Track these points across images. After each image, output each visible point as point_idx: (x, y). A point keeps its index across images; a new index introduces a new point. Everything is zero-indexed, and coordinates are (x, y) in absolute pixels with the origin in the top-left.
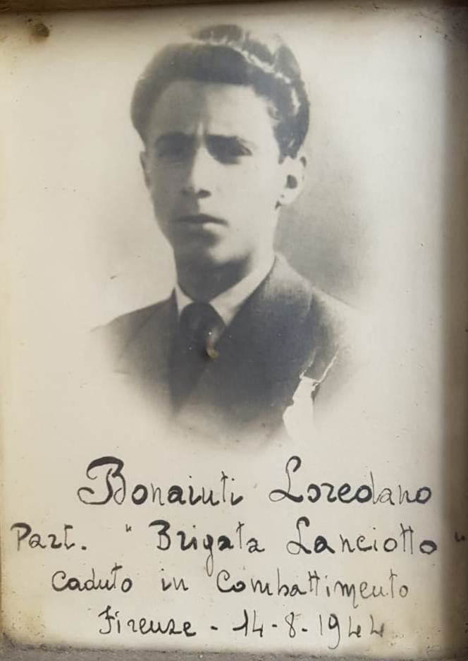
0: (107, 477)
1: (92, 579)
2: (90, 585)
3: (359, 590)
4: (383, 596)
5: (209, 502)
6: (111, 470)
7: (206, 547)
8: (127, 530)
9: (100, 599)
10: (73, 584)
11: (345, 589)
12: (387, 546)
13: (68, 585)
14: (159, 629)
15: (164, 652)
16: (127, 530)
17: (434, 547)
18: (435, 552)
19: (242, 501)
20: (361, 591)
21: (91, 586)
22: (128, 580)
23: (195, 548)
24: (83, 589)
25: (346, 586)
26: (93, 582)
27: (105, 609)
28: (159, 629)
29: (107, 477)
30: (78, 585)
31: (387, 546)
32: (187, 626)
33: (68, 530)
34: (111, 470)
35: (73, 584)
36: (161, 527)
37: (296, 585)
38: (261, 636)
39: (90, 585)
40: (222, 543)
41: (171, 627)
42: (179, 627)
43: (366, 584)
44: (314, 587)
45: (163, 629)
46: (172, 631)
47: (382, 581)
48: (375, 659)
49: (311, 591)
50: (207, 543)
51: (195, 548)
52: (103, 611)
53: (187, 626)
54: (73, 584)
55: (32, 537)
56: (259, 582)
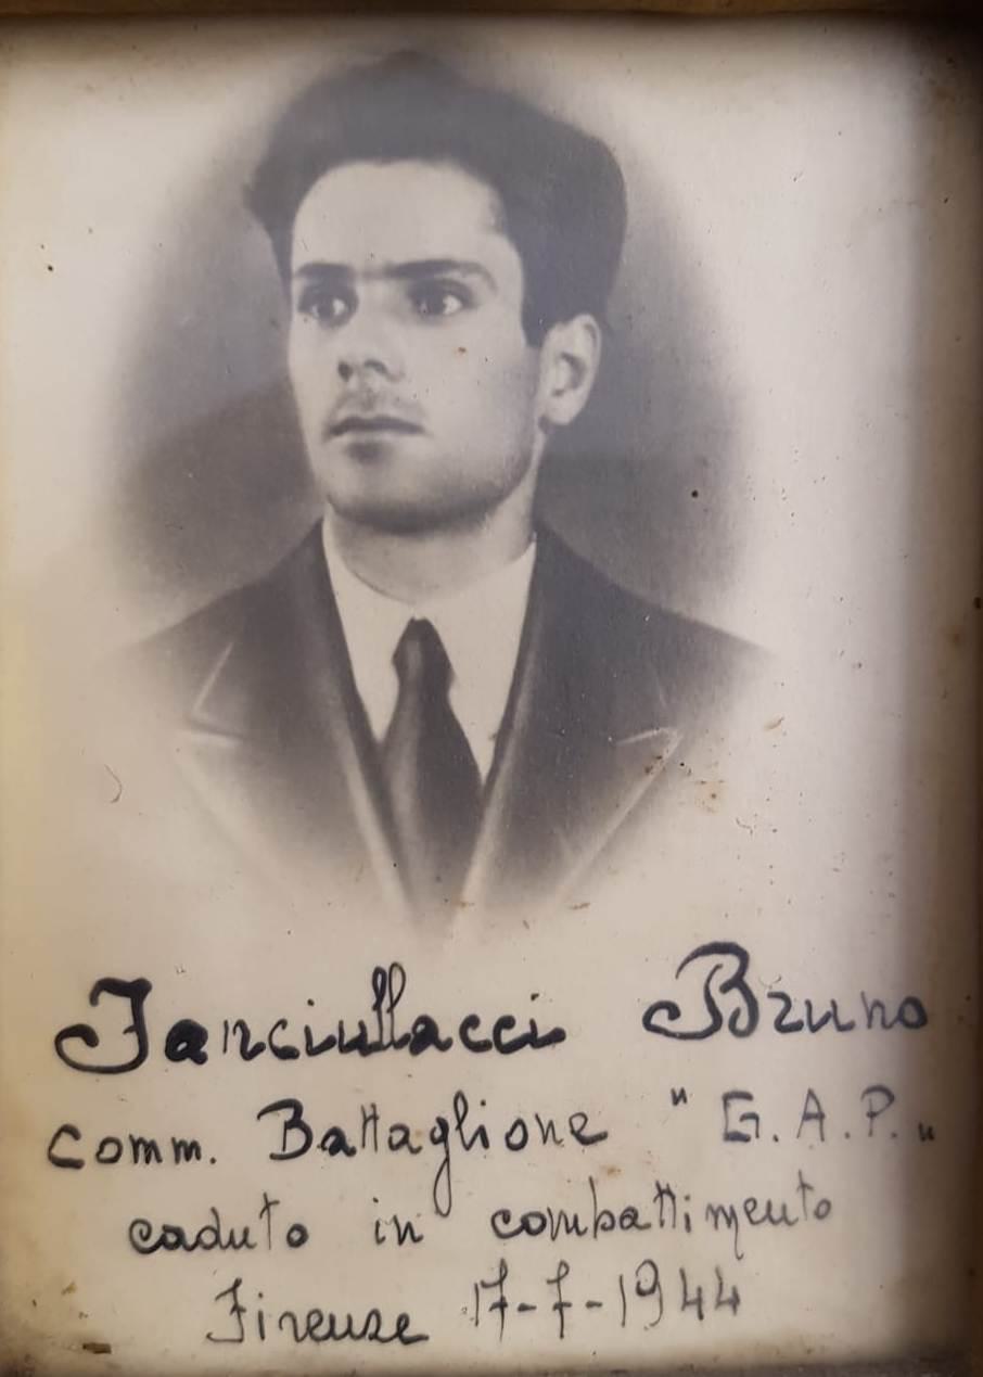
0: (685, 1036)
1: (215, 1226)
2: (208, 1238)
3: (738, 1216)
4: (579, 1233)
5: (831, 1022)
6: (718, 967)
7: (435, 1141)
8: (676, 1101)
9: (222, 1266)
10: (173, 1239)
11: (182, 1150)
12: (55, 1152)
13: (162, 1242)
14: (349, 1332)
15: (972, 1273)
16: (676, 1101)
17: (891, 1098)
18: (893, 1106)
19: (559, 1046)
20: (748, 1214)
21: (214, 1239)
22: (299, 1228)
23: (486, 1144)
24: (226, 1247)
25: (721, 1208)
26: (217, 1232)
27: (230, 1284)
28: (349, 1332)
29: (685, 1036)
30: (180, 1241)
31: (55, 1152)
32: (403, 1322)
33: (808, 1192)
34: (718, 967)
35: (171, 1238)
36: (288, 1114)
37: (710, 1207)
38: (701, 1317)
39: (208, 1238)
40: (331, 1140)
41: (372, 1329)
42: (388, 1330)
43: (755, 1203)
44: (668, 1217)
45: (358, 1329)
46: (375, 1337)
47: (776, 1188)
48: (617, 1372)
49: (662, 1224)
50: (438, 1133)
51: (486, 1144)
52: (225, 1288)
53: (403, 1322)
54: (173, 1239)
55: (459, 1127)
56: (562, 1214)
